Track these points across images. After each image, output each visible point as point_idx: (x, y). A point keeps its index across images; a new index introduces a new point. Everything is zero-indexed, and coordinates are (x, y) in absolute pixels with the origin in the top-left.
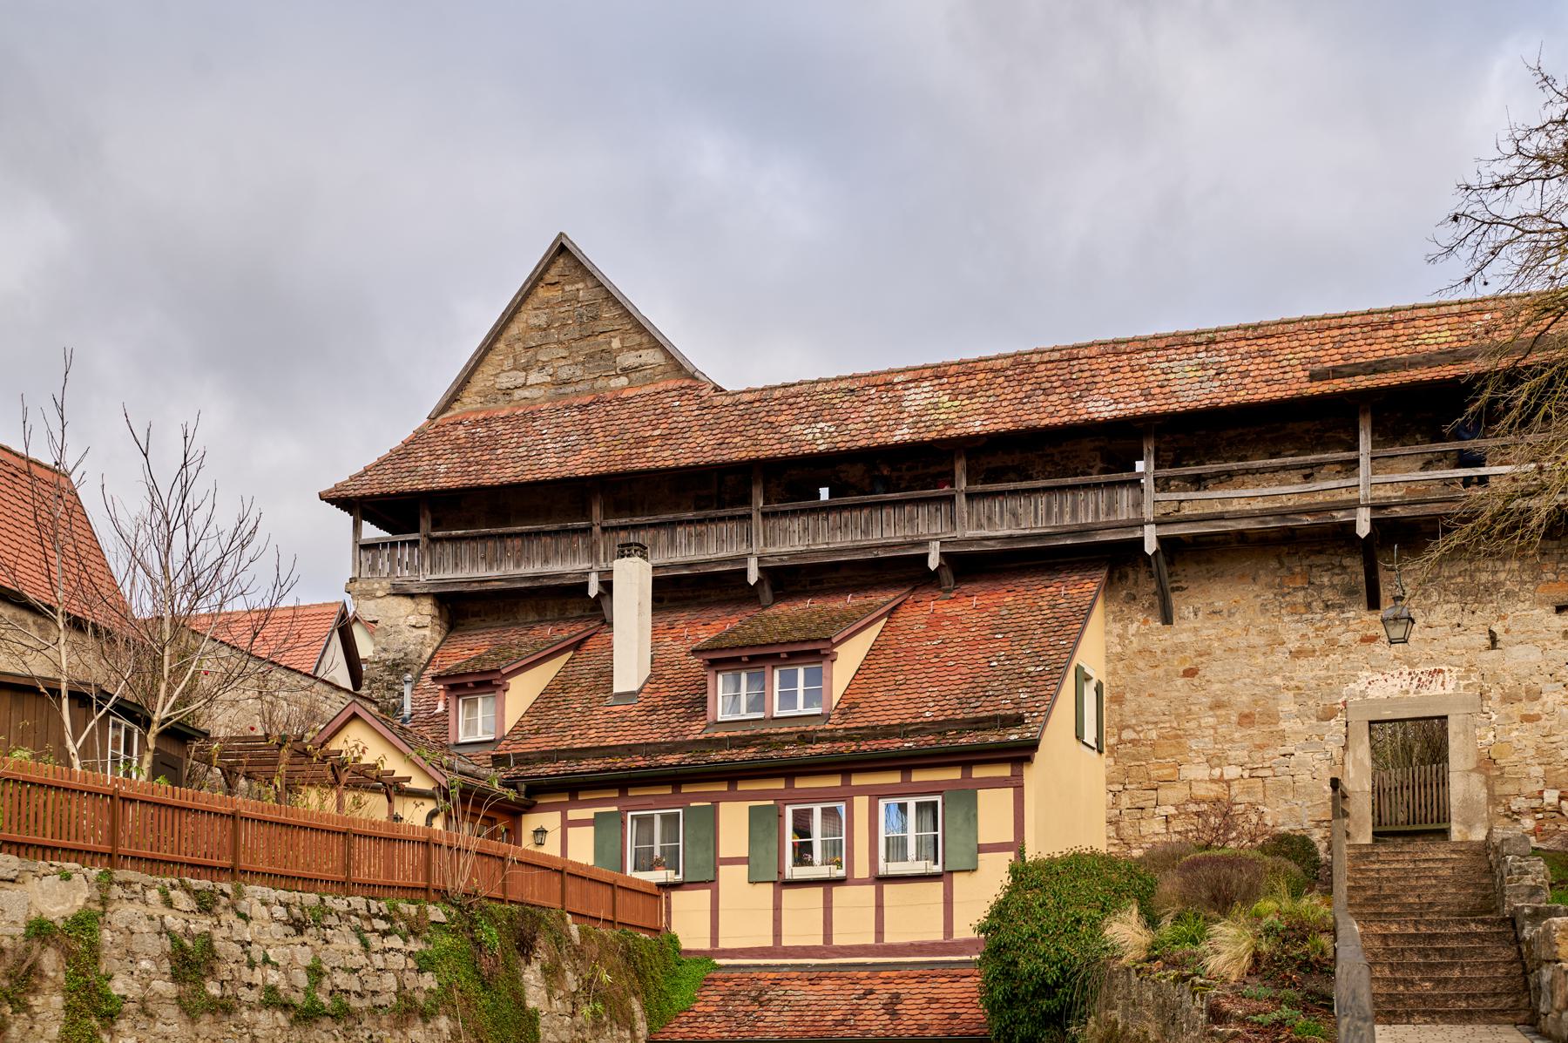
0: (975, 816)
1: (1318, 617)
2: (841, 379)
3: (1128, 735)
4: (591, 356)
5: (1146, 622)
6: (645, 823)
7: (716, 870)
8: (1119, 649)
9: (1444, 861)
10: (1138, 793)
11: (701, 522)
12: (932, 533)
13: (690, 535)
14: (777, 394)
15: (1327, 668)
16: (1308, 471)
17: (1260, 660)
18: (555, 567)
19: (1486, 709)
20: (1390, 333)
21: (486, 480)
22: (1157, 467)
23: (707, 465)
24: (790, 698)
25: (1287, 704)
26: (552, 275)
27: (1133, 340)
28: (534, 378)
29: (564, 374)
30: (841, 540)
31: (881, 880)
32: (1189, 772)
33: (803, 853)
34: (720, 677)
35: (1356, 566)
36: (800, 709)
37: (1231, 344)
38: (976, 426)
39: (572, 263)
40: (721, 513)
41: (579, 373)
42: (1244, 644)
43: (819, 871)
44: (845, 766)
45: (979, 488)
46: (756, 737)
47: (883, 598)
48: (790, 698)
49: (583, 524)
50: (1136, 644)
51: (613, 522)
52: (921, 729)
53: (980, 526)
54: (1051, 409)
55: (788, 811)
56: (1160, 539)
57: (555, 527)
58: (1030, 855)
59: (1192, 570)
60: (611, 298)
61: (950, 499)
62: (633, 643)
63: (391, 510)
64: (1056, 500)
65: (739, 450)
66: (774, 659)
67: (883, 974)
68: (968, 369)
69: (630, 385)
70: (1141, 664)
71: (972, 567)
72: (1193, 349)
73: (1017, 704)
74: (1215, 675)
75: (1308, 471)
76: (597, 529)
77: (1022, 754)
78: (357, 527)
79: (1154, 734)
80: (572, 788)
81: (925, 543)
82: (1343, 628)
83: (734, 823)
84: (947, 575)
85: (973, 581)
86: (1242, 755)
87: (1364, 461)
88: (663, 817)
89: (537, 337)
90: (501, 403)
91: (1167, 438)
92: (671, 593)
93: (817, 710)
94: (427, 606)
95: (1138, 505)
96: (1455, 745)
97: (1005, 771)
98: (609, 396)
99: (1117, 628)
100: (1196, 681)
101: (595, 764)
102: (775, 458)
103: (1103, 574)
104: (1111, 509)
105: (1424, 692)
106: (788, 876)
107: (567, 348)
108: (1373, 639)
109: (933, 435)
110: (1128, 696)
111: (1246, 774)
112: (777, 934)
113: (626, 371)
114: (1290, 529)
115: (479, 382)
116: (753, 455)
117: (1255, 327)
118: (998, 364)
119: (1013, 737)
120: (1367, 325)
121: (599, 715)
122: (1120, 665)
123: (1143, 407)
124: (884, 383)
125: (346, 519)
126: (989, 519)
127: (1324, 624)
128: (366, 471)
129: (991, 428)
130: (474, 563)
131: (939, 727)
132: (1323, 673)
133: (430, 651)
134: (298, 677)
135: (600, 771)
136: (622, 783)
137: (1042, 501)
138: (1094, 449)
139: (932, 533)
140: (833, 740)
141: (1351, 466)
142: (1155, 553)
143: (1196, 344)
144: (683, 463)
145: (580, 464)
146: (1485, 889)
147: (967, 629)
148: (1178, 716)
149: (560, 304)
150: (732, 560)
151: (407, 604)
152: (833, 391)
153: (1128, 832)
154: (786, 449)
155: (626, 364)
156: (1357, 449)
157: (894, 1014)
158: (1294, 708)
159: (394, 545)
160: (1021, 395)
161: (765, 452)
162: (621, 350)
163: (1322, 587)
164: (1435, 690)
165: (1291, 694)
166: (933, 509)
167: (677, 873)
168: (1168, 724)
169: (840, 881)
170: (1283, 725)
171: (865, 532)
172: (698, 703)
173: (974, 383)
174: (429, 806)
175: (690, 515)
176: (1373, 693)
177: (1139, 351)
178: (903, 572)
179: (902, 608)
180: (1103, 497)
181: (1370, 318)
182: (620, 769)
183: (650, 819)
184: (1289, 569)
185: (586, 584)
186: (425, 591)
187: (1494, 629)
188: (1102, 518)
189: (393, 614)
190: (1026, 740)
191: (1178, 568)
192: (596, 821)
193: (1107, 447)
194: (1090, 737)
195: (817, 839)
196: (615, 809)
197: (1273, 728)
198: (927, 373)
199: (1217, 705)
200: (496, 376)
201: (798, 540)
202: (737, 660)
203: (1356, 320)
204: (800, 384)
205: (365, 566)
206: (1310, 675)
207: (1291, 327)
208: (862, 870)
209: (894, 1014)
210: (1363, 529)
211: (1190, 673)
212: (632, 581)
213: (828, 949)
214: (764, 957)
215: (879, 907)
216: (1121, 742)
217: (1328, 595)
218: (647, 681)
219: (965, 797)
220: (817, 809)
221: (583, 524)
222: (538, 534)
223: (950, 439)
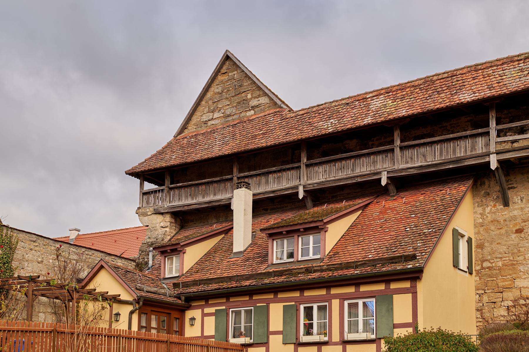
0: (392, 309)
3: (486, 264)
4: (239, 103)
5: (495, 206)
6: (238, 314)
7: (268, 338)
8: (481, 220)
10: (492, 295)
11: (279, 171)
13: (275, 178)
14: (314, 109)
18: (218, 197)
21: (189, 160)
22: (497, 124)
24: (310, 250)
26: (224, 70)
27: (485, 63)
28: (216, 115)
29: (228, 112)
30: (341, 175)
31: (345, 343)
33: (308, 332)
34: (275, 242)
36: (311, 256)
38: (403, 113)
39: (232, 63)
41: (234, 111)
44: (328, 284)
45: (406, 144)
46: (286, 271)
47: (361, 202)
48: (310, 250)
49: (229, 177)
50: (490, 217)
51: (242, 175)
52: (364, 264)
53: (407, 162)
54: (441, 100)
55: (302, 307)
56: (499, 161)
57: (218, 179)
58: (421, 328)
59: (519, 178)
60: (247, 76)
61: (392, 150)
62: (243, 229)
63: (156, 175)
65: (295, 136)
66: (297, 232)
68: (402, 87)
69: (255, 114)
70: (492, 228)
71: (404, 183)
72: (517, 63)
73: (415, 249)
77: (415, 275)
78: (142, 185)
79: (500, 264)
80: (206, 298)
81: (380, 173)
83: (276, 313)
84: (392, 188)
85: (406, 190)
88: (245, 311)
89: (217, 97)
90: (203, 128)
91: (506, 112)
92: (260, 206)
93: (318, 257)
94: (168, 218)
95: (487, 145)
97: (407, 285)
98: (245, 119)
99: (480, 210)
100: (522, 235)
101: (214, 286)
103: (470, 182)
104: (473, 148)
106: (346, 339)
107: (230, 100)
109: (382, 119)
110: (486, 244)
113: (253, 108)
115: (195, 119)
116: (300, 137)
119: (409, 267)
121: (225, 263)
122: (481, 229)
124: (362, 99)
126: (412, 158)
129: (410, 112)
130: (186, 197)
131: (373, 262)
134: (83, 250)
135: (216, 289)
136: (227, 295)
137: (438, 147)
138: (468, 121)
139: (382, 167)
140: (322, 271)
142: (497, 168)
145: (226, 150)
147: (398, 214)
148: (513, 254)
149: (227, 81)
150: (292, 188)
151: (160, 217)
152: (339, 105)
153: (487, 315)
154: (315, 133)
155: (253, 105)
160: (427, 95)
161: (305, 136)
162: (251, 99)
166: (384, 156)
167: (251, 339)
168: (508, 258)
169: (325, 343)
171: (353, 170)
172: (264, 257)
173: (405, 93)
174: (130, 308)
175: (274, 169)
177: (488, 68)
178: (369, 188)
179: (370, 206)
180: (469, 143)
182: (224, 288)
183: (240, 312)
186: (166, 211)
188: (469, 153)
189: (154, 222)
190: (416, 267)
191: (512, 177)
192: (216, 314)
194: (463, 264)
196: (224, 307)
198: (382, 92)
200: (201, 116)
201: (323, 175)
202: (280, 233)
204: (325, 104)
205: (145, 201)
208: (336, 338)
211: (519, 231)
212: (241, 200)
216: (483, 268)
218: (249, 246)
219: (386, 301)
220: (315, 306)
221: (229, 177)
222: (212, 182)
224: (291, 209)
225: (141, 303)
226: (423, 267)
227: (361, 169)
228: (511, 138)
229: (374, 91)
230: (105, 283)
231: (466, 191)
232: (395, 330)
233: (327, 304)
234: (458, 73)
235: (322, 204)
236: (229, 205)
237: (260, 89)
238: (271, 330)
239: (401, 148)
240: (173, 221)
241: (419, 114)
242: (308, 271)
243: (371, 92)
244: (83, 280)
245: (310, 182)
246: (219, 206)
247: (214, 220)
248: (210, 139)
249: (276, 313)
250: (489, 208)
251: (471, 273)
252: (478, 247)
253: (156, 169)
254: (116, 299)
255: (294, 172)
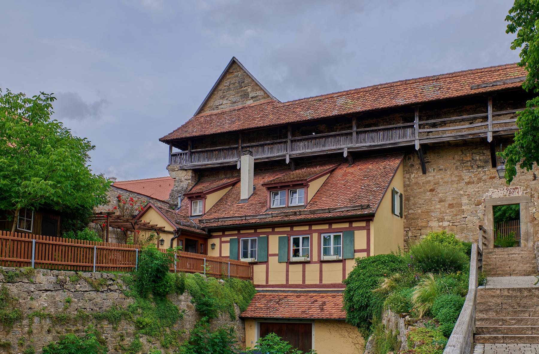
1: (475, 170)
2: (317, 97)
6: (245, 242)
7: (268, 258)
9: (519, 254)
10: (414, 231)
11: (272, 144)
12: (345, 146)
14: (297, 102)
15: (478, 188)
16: (471, 121)
17: (455, 186)
19: (533, 201)
20: (498, 73)
21: (207, 133)
23: (273, 125)
25: (465, 200)
32: (431, 224)
33: (296, 253)
35: (488, 153)
37: (444, 80)
38: (359, 109)
40: (280, 141)
42: (450, 180)
43: (301, 259)
44: (310, 223)
49: (236, 146)
50: (414, 181)
51: (245, 145)
53: (361, 142)
55: (292, 238)
56: (421, 145)
60: (249, 76)
61: (351, 134)
63: (183, 143)
64: (386, 132)
65: (285, 120)
67: (310, 294)
68: (357, 91)
70: (415, 188)
71: (358, 157)
74: (441, 192)
75: (471, 121)
76: (240, 147)
77: (369, 218)
78: (171, 149)
80: (223, 230)
81: (343, 149)
82: (484, 174)
83: (274, 242)
86: (449, 218)
87: (490, 116)
91: (424, 112)
92: (260, 168)
94: (190, 173)
95: (413, 134)
96: (522, 214)
97: (363, 224)
100: (434, 193)
102: (294, 122)
104: (404, 136)
105: (512, 195)
106: (322, 259)
108: (494, 178)
109: (345, 112)
111: (451, 225)
112: (287, 280)
114: (465, 140)
117: (452, 74)
118: (367, 89)
119: (366, 212)
120: (491, 71)
123: (414, 100)
124: (331, 97)
125: (168, 146)
127: (477, 173)
128: (174, 131)
129: (364, 109)
130: (204, 160)
132: (477, 190)
133: (191, 187)
134: (136, 195)
138: (400, 117)
141: (486, 118)
143: (432, 80)
144: (265, 125)
145: (235, 127)
146: (533, 264)
147: (355, 177)
150: (281, 156)
151: (185, 172)
154: (298, 119)
156: (487, 112)
157: (322, 309)
158: (467, 201)
159: (181, 154)
161: (291, 120)
163: (476, 160)
164: (516, 194)
165: (466, 197)
166: (345, 137)
169: (308, 262)
170: (463, 208)
174: (172, 236)
175: (268, 142)
176: (494, 196)
178: (336, 159)
180: (401, 132)
181: (491, 69)
184: (465, 154)
185: (236, 165)
187: (535, 173)
190: (370, 213)
192: (231, 241)
193: (404, 114)
194: (397, 212)
195: (332, 246)
196: (236, 237)
197: (460, 208)
199: (441, 201)
203: (486, 70)
206: (473, 190)
207: (464, 73)
208: (315, 258)
209: (322, 309)
210: (490, 139)
212: (246, 163)
213: (304, 285)
214: (283, 288)
215: (321, 271)
217: (479, 163)
219: (350, 234)
223: (350, 113)
224: (280, 171)
225: (180, 233)
226: (375, 213)
227: (330, 146)
228: (428, 130)
229: (338, 93)
230: (153, 218)
231: (400, 163)
232: (355, 254)
233: (309, 236)
234: (395, 85)
235: (302, 168)
236: (353, 160)
237: (257, 86)
238: (270, 253)
239: (358, 133)
240: (194, 175)
241: (370, 110)
242: (295, 214)
243: (337, 93)
244: (136, 216)
245: (294, 152)
246: (212, 168)
247: (223, 176)
248: (221, 119)
249: (274, 242)
250: (413, 175)
251: (401, 217)
252: (406, 200)
253: (182, 138)
254: (161, 230)
255: (282, 145)
